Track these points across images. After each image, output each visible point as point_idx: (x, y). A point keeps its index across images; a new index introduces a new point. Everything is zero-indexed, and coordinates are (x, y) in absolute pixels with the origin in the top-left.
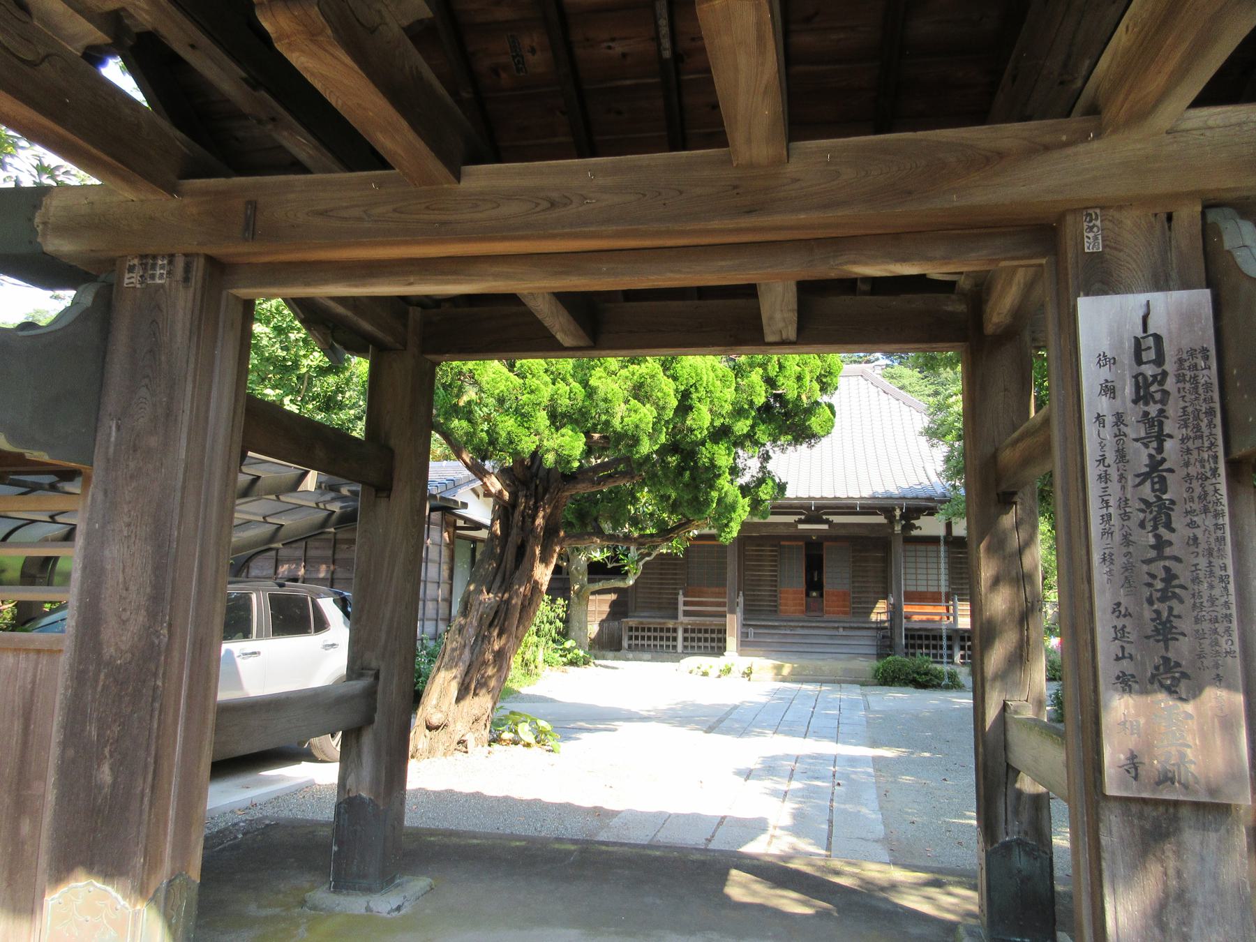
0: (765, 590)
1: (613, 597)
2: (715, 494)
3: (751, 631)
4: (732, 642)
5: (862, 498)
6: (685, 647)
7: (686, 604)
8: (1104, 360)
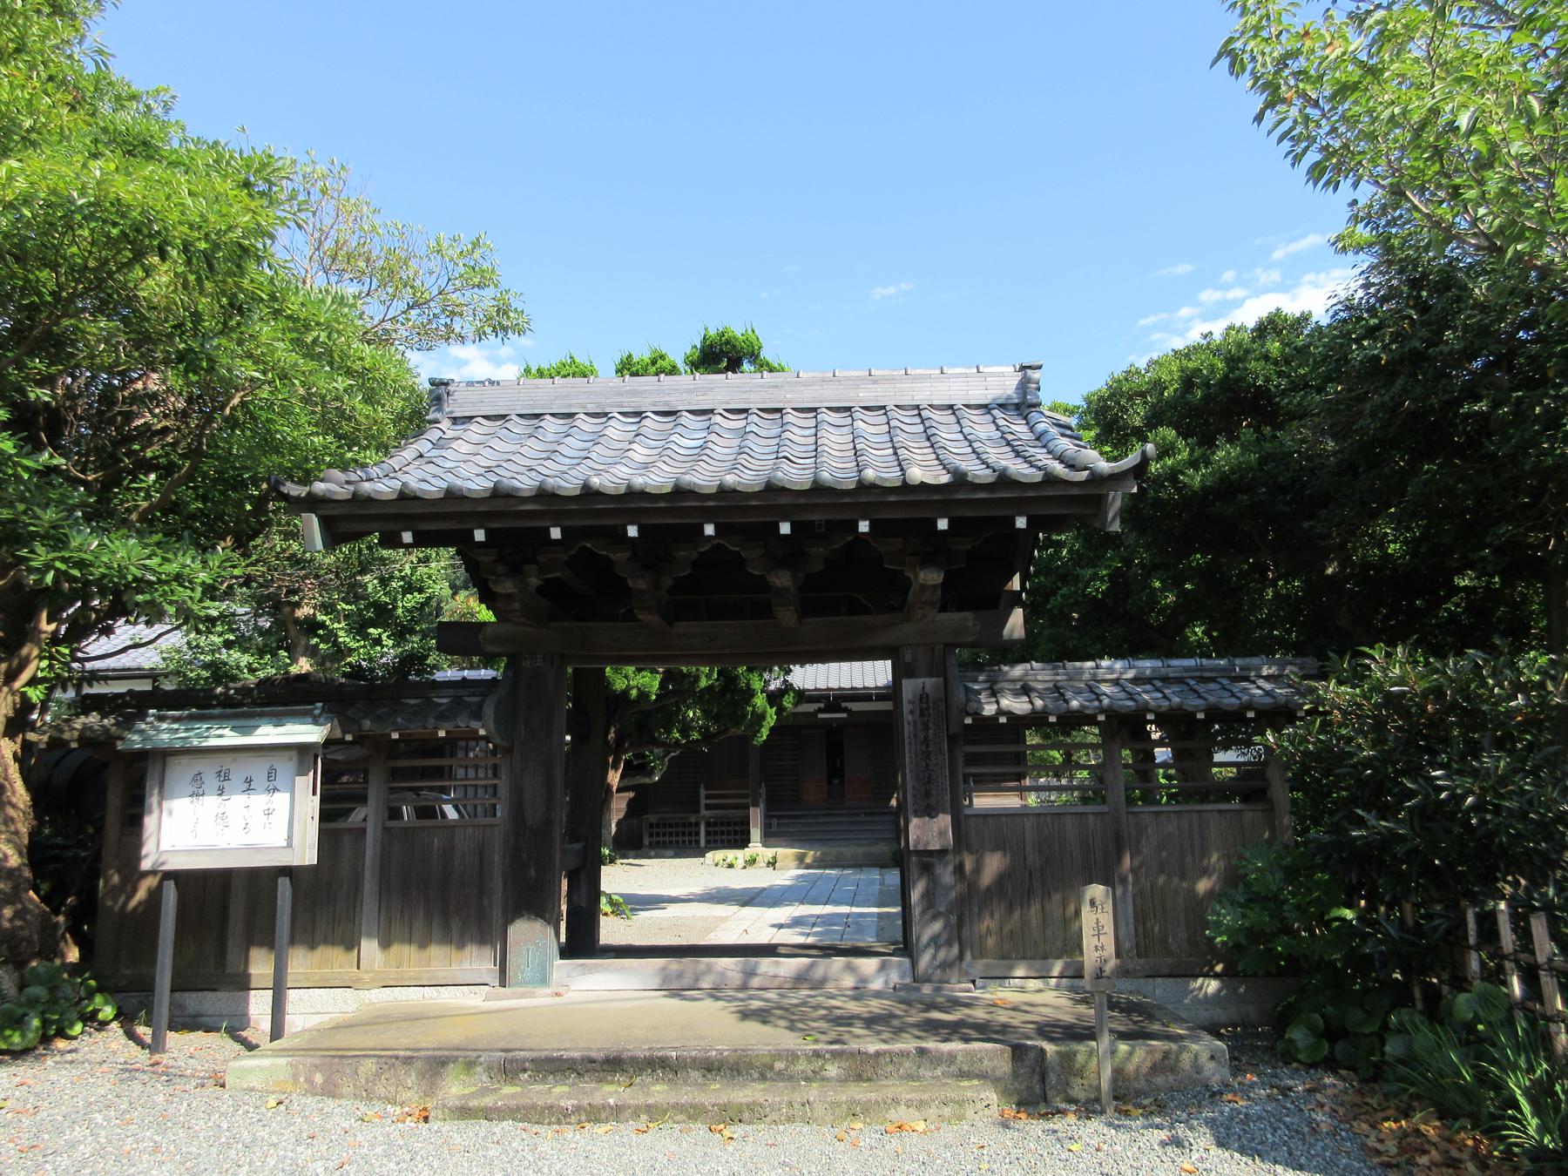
1: (632, 795)
2: (750, 709)
3: (775, 821)
4: (756, 833)
5: (877, 688)
6: (708, 842)
7: (707, 797)
8: (910, 702)
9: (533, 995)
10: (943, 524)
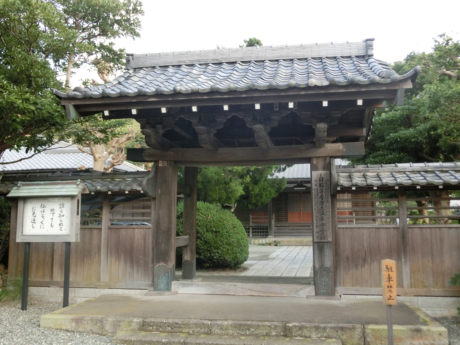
0: (283, 213)
6: (253, 235)
7: (338, 218)
8: (315, 181)
9: (163, 295)
10: (325, 104)
